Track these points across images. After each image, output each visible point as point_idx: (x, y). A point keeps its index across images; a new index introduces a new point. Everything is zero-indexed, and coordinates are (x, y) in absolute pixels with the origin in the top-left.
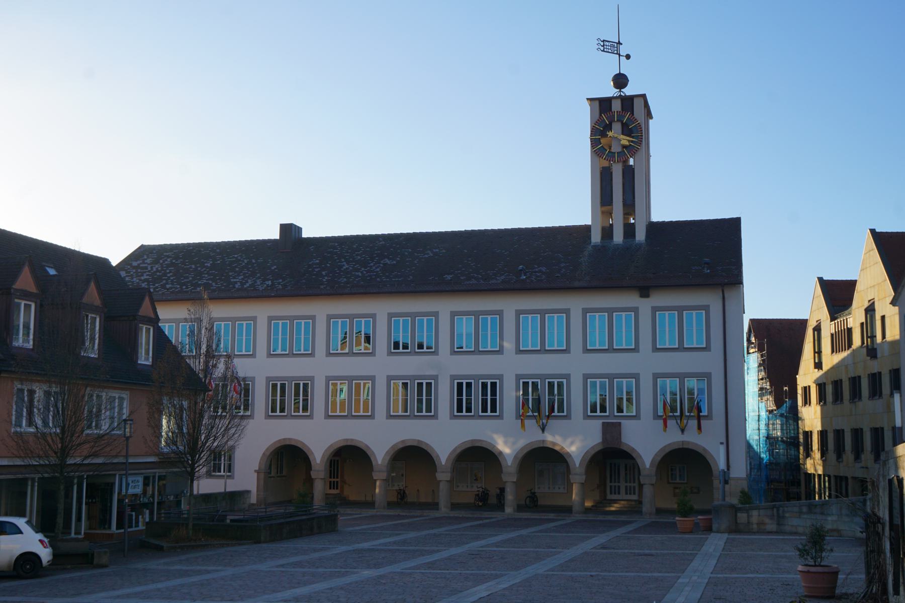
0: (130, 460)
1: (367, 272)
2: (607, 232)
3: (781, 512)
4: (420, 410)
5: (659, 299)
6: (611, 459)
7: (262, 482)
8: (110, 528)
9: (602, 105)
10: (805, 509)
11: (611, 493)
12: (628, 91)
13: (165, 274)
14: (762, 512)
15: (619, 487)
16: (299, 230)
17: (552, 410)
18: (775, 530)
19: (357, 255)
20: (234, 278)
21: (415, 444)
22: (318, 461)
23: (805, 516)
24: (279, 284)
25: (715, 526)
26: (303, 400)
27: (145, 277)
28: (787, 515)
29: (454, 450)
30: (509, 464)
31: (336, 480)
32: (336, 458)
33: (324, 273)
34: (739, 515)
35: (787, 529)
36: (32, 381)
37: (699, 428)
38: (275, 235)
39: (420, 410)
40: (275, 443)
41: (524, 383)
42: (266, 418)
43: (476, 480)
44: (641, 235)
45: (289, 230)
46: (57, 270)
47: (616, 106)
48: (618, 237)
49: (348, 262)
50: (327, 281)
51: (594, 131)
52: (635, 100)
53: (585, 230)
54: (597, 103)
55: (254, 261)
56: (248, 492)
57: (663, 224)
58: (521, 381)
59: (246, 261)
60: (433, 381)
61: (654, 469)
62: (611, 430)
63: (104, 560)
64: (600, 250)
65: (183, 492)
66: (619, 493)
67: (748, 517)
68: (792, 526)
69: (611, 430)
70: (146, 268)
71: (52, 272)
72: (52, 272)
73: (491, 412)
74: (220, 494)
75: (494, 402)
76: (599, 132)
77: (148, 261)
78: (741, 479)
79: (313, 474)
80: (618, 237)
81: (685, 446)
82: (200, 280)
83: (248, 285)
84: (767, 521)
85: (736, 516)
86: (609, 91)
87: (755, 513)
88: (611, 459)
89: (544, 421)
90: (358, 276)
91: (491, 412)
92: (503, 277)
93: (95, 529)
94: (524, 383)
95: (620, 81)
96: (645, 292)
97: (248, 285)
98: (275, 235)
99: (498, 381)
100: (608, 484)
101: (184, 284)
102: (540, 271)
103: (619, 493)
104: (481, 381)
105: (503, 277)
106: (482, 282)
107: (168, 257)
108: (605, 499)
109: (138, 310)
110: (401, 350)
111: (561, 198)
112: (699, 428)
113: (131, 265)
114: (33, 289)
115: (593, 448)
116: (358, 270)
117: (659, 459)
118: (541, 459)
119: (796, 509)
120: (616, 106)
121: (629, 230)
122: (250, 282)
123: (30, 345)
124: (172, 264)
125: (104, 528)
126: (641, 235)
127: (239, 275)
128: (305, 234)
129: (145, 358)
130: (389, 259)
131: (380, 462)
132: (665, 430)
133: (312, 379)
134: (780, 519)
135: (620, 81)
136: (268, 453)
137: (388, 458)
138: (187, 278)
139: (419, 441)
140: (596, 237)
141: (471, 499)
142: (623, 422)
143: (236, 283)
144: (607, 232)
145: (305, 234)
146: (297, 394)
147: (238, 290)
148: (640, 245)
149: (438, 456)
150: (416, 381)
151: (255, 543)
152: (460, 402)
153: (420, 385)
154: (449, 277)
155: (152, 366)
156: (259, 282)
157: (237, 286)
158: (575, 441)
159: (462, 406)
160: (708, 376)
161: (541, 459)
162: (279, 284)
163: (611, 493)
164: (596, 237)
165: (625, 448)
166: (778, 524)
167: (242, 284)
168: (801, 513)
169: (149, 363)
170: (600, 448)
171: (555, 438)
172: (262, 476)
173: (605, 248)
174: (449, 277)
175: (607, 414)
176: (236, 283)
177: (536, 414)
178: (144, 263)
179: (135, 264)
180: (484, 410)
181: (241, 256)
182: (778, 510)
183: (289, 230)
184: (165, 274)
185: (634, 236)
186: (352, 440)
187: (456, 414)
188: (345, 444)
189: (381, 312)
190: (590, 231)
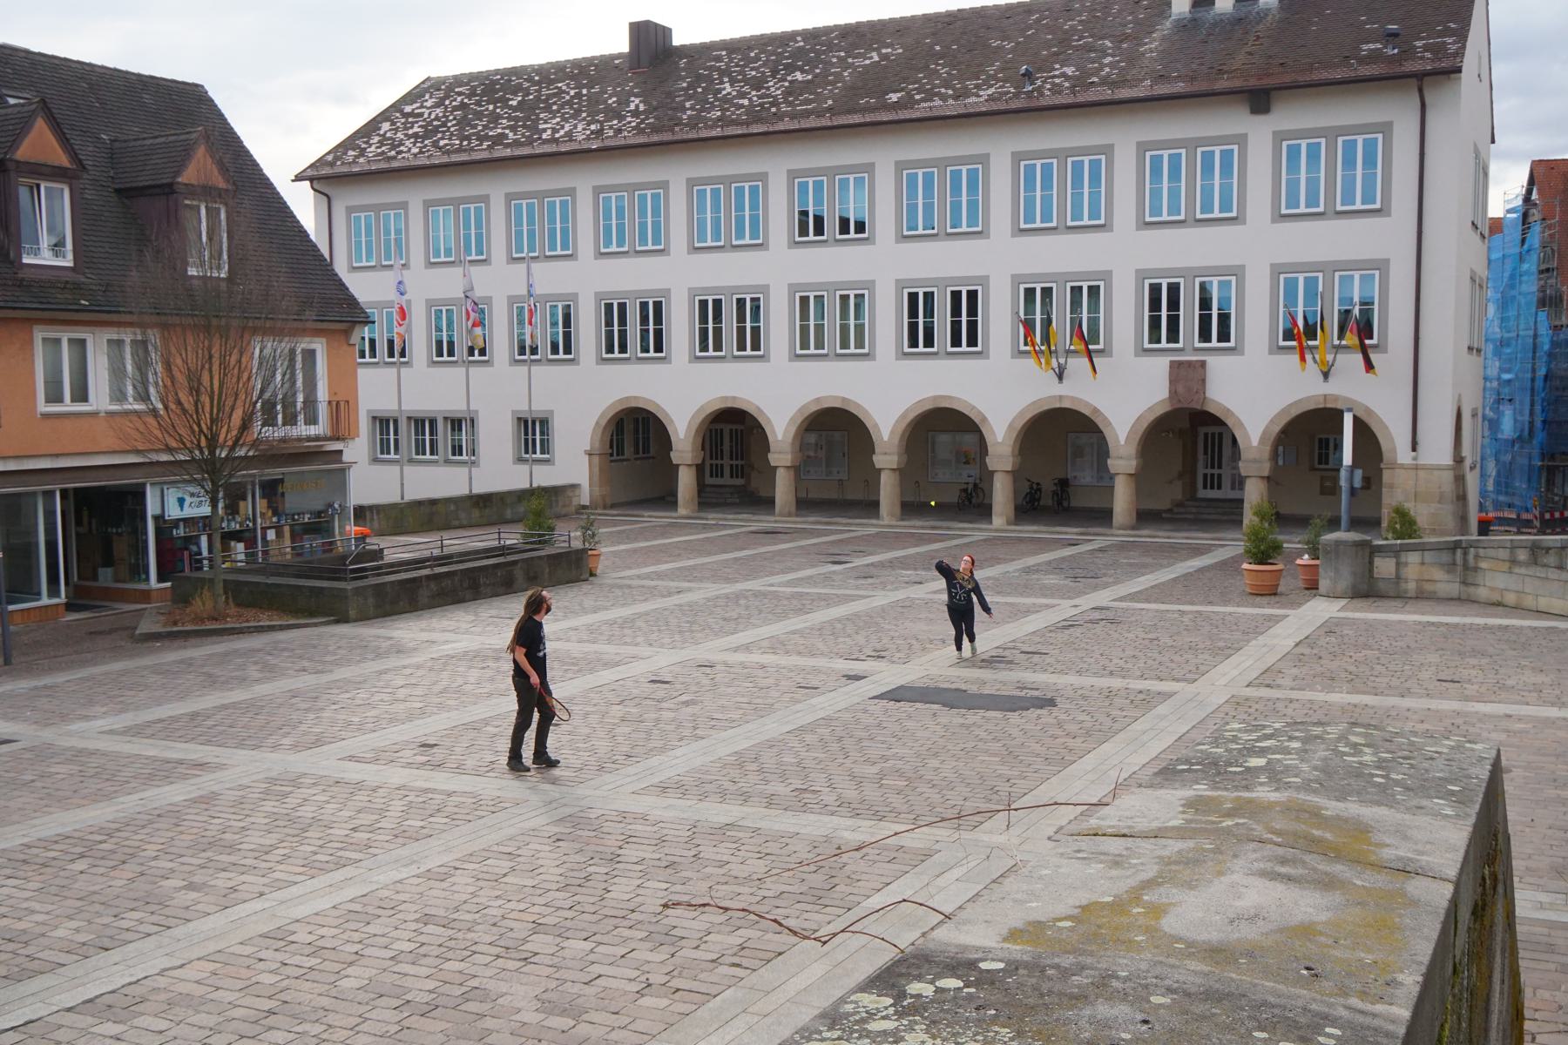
1: (759, 97)
3: (1471, 557)
7: (596, 470)
8: (147, 579)
10: (1522, 555)
11: (1205, 487)
13: (444, 124)
14: (1429, 556)
15: (1220, 476)
16: (666, 32)
18: (1455, 594)
22: (682, 436)
23: (1523, 570)
25: (1324, 584)
27: (416, 129)
28: (1483, 565)
29: (903, 416)
33: (688, 105)
34: (1378, 561)
35: (1482, 593)
37: (1369, 366)
41: (1027, 290)
42: (790, 360)
43: (967, 463)
49: (733, 82)
50: (690, 117)
55: (584, 91)
56: (574, 487)
58: (1022, 287)
62: (1187, 376)
65: (331, 505)
66: (1219, 487)
67: (1398, 564)
68: (1492, 589)
69: (1187, 376)
70: (421, 115)
73: (816, 348)
75: (972, 326)
78: (1439, 468)
79: (675, 457)
84: (1439, 574)
85: (1371, 563)
87: (1413, 558)
89: (1062, 361)
90: (742, 106)
91: (816, 348)
92: (990, 91)
93: (124, 582)
94: (1027, 290)
96: (1260, 101)
97: (562, 132)
98: (620, 44)
99: (979, 289)
100: (1201, 471)
101: (468, 138)
102: (1064, 75)
103: (1219, 487)
105: (990, 91)
106: (951, 101)
107: (460, 94)
108: (1193, 498)
109: (178, 173)
110: (852, 235)
112: (1369, 366)
113: (401, 111)
116: (742, 95)
118: (1061, 434)
119: (1504, 554)
122: (567, 128)
124: (463, 106)
125: (139, 580)
128: (677, 41)
130: (803, 72)
131: (780, 437)
134: (1468, 573)
137: (793, 429)
138: (475, 127)
139: (844, 399)
141: (953, 497)
143: (545, 130)
145: (677, 41)
147: (546, 142)
149: (876, 425)
151: (337, 622)
152: (913, 328)
153: (845, 298)
154: (894, 97)
156: (580, 128)
158: (1125, 393)
160: (1382, 266)
161: (1061, 434)
163: (1205, 487)
166: (1464, 583)
167: (555, 131)
168: (1514, 562)
169: (67, 261)
170: (1167, 408)
171: (1083, 389)
174: (894, 97)
175: (1180, 345)
176: (545, 130)
179: (408, 109)
180: (956, 342)
182: (1465, 554)
184: (444, 124)
188: (723, 406)
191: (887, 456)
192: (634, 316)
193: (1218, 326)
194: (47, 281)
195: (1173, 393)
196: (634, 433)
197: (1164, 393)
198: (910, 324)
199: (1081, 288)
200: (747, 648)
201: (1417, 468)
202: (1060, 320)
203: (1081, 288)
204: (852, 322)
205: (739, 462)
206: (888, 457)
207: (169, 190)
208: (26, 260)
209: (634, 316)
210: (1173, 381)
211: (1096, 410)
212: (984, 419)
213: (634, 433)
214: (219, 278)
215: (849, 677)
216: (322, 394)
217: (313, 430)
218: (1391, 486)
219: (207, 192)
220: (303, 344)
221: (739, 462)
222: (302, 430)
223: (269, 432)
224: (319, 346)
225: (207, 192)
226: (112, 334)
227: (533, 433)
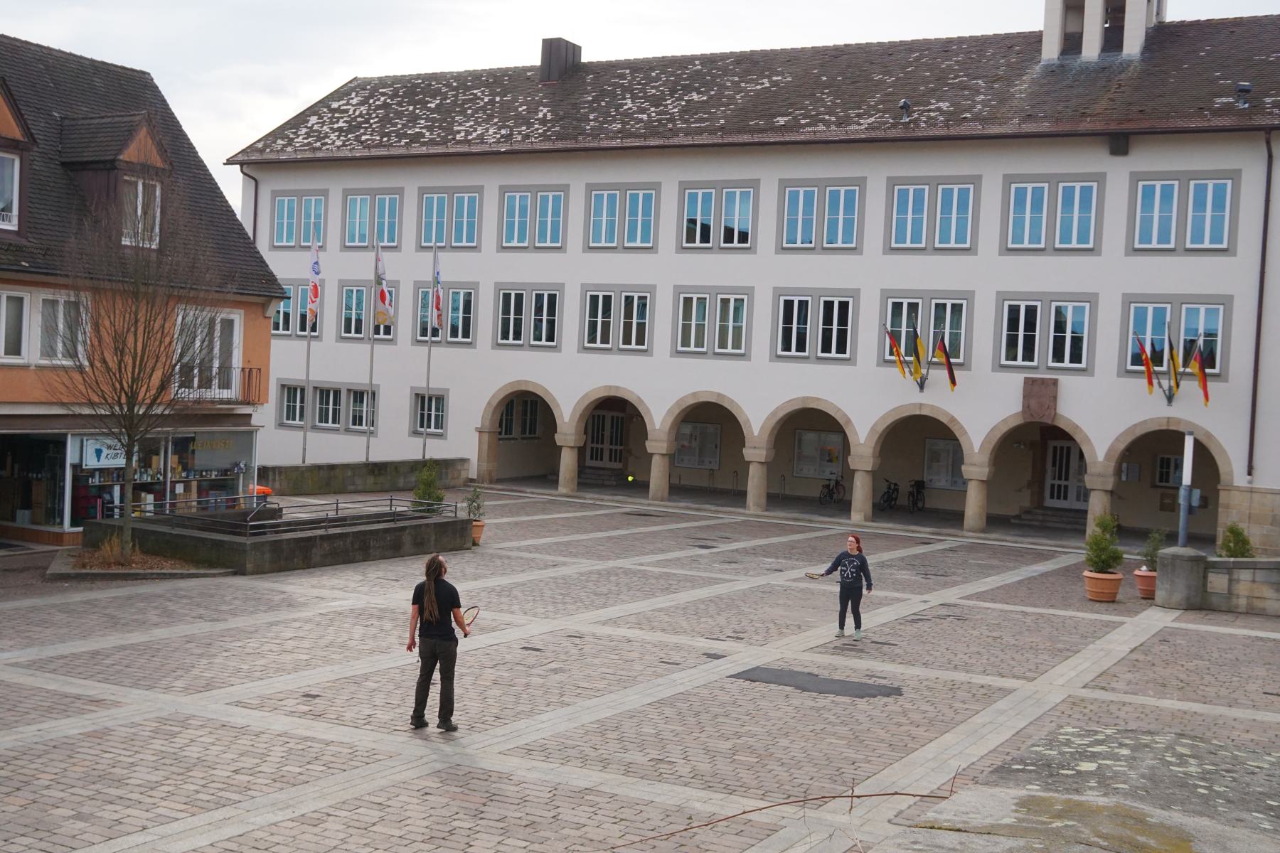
1: (658, 114)
2: (1072, 43)
4: (723, 344)
5: (1144, 160)
6: (1040, 447)
7: (485, 447)
8: (62, 523)
11: (1052, 497)
13: (367, 121)
14: (1260, 575)
15: (1066, 487)
16: (576, 50)
19: (653, 88)
20: (460, 125)
21: (944, 420)
22: (566, 420)
24: (520, 133)
25: (1160, 595)
26: (548, 321)
27: (341, 124)
30: (862, 441)
31: (600, 446)
32: (601, 413)
33: (591, 116)
39: (723, 344)
40: (506, 386)
41: (722, 300)
43: (830, 461)
44: (1133, 44)
45: (559, 54)
49: (633, 99)
53: (1033, 41)
55: (498, 99)
56: (464, 461)
57: (1182, 25)
59: (486, 99)
60: (745, 297)
61: (1112, 464)
62: (1040, 393)
64: (1054, 72)
65: (237, 465)
66: (1065, 498)
67: (1230, 581)
69: (1040, 393)
74: (296, 468)
77: (354, 102)
80: (1091, 49)
81: (1173, 428)
82: (410, 128)
83: (474, 135)
85: (1205, 577)
87: (1245, 575)
88: (1040, 447)
90: (641, 121)
92: (871, 120)
93: (39, 524)
96: (1119, 143)
97: (474, 135)
98: (532, 57)
100: (1049, 481)
101: (388, 135)
102: (939, 110)
104: (823, 299)
105: (871, 120)
106: (834, 128)
107: (383, 94)
109: (120, 151)
115: (1005, 421)
116: (642, 111)
117: (1122, 446)
121: (1113, 38)
122: (480, 131)
126: (1133, 44)
127: (468, 121)
128: (585, 58)
130: (699, 93)
132: (1151, 392)
133: (750, 291)
136: (495, 403)
137: (670, 420)
139: (719, 395)
141: (815, 492)
142: (1064, 379)
143: (459, 132)
144: (1072, 43)
145: (585, 58)
146: (539, 310)
147: (459, 142)
148: (1129, 63)
149: (748, 421)
150: (720, 297)
151: (235, 574)
154: (782, 121)
157: (458, 137)
158: (981, 406)
159: (689, 338)
160: (1226, 301)
161: (919, 442)
162: (520, 133)
164: (1051, 51)
170: (1019, 421)
171: (939, 399)
172: (486, 437)
174: (782, 121)
176: (459, 132)
177: (911, 359)
178: (348, 104)
179: (335, 105)
181: (483, 92)
183: (559, 54)
184: (367, 121)
185: (1119, 46)
186: (617, 388)
187: (780, 352)
189: (763, 190)
190: (1041, 41)
191: (756, 450)
193: (1071, 348)
195: (1026, 407)
196: (522, 415)
198: (609, 317)
200: (614, 622)
201: (1251, 491)
205: (619, 448)
206: (757, 452)
210: (1027, 395)
211: (953, 419)
212: (849, 421)
213: (522, 415)
216: (237, 361)
217: (225, 394)
218: (1227, 507)
220: (223, 314)
221: (619, 448)
222: (216, 393)
223: (184, 393)
224: (238, 317)
225: (144, 170)
226: (48, 294)
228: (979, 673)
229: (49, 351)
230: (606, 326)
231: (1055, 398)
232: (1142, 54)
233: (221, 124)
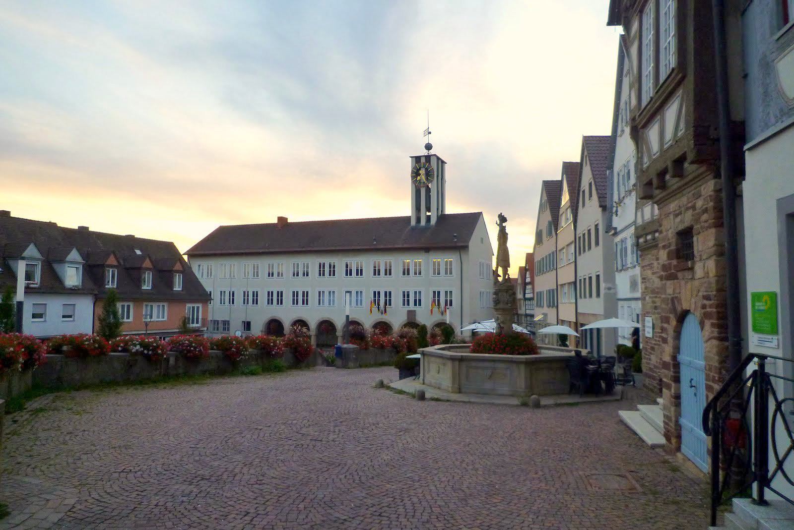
0: (148, 332)
2: (418, 220)
9: (417, 159)
12: (432, 152)
16: (286, 219)
17: (446, 305)
36: (129, 301)
38: (275, 221)
45: (282, 220)
46: (141, 251)
47: (423, 160)
48: (423, 222)
51: (413, 172)
52: (432, 158)
53: (407, 219)
54: (414, 158)
62: (411, 314)
63: (37, 341)
64: (413, 229)
69: (411, 314)
71: (138, 252)
72: (138, 252)
76: (416, 173)
80: (423, 222)
86: (424, 152)
95: (429, 147)
98: (275, 221)
111: (400, 206)
114: (115, 263)
120: (423, 160)
123: (115, 286)
128: (289, 221)
129: (178, 287)
135: (429, 147)
140: (413, 222)
141: (769, 358)
144: (418, 220)
145: (289, 221)
155: (182, 291)
164: (413, 222)
165: (418, 323)
169: (180, 289)
173: (417, 230)
183: (280, 219)
192: (300, 301)
193: (418, 302)
194: (147, 292)
197: (406, 318)
198: (385, 299)
199: (438, 274)
202: (382, 300)
203: (438, 274)
204: (388, 298)
207: (140, 268)
208: (174, 289)
209: (300, 301)
214: (113, 288)
215: (371, 312)
216: (200, 317)
217: (198, 325)
219: (177, 272)
220: (196, 305)
222: (195, 325)
223: (191, 325)
224: (200, 305)
225: (177, 272)
226: (158, 304)
227: (247, 325)
228: (311, 340)
229: (158, 317)
230: (303, 296)
231: (415, 315)
232: (435, 224)
233: (183, 247)
